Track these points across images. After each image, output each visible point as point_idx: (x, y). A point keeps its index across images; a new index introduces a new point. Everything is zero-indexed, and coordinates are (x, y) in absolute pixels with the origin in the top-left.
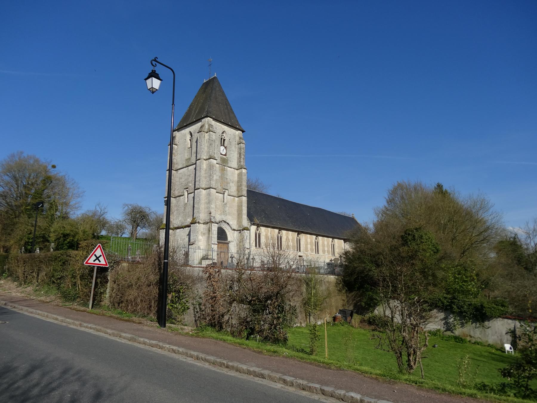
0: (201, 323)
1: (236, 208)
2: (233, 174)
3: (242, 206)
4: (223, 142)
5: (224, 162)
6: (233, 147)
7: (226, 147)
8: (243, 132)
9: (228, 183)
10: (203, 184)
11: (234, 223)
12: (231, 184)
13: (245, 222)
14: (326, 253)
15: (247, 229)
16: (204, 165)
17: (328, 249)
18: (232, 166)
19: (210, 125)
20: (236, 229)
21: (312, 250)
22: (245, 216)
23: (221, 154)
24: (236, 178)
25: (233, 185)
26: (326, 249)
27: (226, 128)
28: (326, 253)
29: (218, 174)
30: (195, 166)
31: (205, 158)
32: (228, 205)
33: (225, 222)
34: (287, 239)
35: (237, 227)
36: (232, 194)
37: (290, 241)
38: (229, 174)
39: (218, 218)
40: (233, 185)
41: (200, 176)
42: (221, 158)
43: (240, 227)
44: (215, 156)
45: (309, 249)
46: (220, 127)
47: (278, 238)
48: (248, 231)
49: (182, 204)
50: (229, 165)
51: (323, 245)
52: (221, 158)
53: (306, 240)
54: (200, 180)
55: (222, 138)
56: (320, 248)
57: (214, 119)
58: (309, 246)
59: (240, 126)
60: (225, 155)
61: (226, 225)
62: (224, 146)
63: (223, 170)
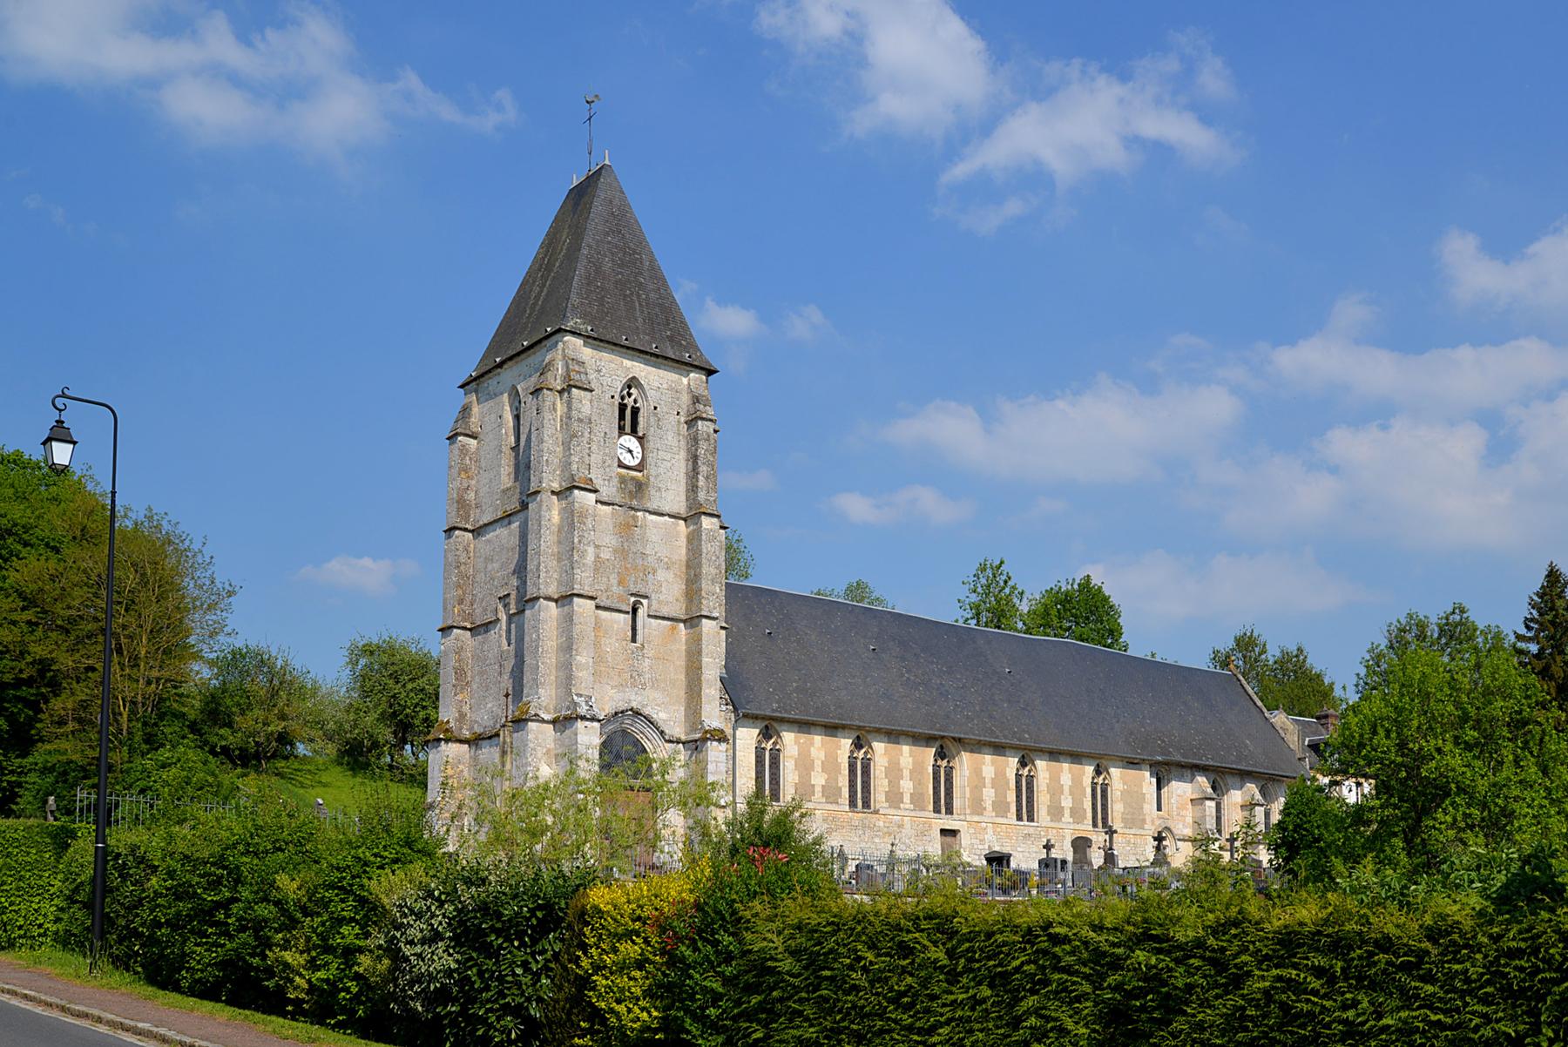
0: (470, 968)
1: (681, 662)
2: (664, 539)
3: (700, 653)
4: (629, 419)
5: (635, 488)
6: (670, 436)
7: (641, 439)
8: (710, 372)
9: (647, 571)
10: (548, 581)
11: (672, 718)
12: (661, 575)
13: (715, 714)
14: (1067, 818)
15: (721, 737)
16: (551, 512)
17: (1077, 802)
18: (666, 509)
19: (572, 361)
20: (683, 738)
21: (917, 800)
22: (712, 692)
23: (621, 465)
24: (684, 551)
25: (670, 576)
26: (1067, 803)
27: (638, 369)
28: (1067, 818)
29: (609, 540)
30: (505, 536)
31: (556, 486)
32: (649, 652)
33: (637, 713)
34: (894, 772)
35: (687, 734)
36: (665, 612)
37: (906, 773)
38: (653, 535)
39: (607, 700)
40: (670, 576)
41: (538, 553)
42: (623, 480)
43: (693, 729)
44: (597, 478)
45: (988, 804)
46: (610, 370)
47: (1018, 783)
48: (724, 746)
49: (492, 655)
50: (652, 506)
51: (1055, 790)
52: (623, 480)
53: (977, 772)
54: (538, 569)
55: (622, 408)
56: (880, 784)
57: (589, 339)
58: (989, 794)
59: (692, 346)
60: (640, 468)
61: (649, 731)
62: (634, 431)
63: (627, 530)
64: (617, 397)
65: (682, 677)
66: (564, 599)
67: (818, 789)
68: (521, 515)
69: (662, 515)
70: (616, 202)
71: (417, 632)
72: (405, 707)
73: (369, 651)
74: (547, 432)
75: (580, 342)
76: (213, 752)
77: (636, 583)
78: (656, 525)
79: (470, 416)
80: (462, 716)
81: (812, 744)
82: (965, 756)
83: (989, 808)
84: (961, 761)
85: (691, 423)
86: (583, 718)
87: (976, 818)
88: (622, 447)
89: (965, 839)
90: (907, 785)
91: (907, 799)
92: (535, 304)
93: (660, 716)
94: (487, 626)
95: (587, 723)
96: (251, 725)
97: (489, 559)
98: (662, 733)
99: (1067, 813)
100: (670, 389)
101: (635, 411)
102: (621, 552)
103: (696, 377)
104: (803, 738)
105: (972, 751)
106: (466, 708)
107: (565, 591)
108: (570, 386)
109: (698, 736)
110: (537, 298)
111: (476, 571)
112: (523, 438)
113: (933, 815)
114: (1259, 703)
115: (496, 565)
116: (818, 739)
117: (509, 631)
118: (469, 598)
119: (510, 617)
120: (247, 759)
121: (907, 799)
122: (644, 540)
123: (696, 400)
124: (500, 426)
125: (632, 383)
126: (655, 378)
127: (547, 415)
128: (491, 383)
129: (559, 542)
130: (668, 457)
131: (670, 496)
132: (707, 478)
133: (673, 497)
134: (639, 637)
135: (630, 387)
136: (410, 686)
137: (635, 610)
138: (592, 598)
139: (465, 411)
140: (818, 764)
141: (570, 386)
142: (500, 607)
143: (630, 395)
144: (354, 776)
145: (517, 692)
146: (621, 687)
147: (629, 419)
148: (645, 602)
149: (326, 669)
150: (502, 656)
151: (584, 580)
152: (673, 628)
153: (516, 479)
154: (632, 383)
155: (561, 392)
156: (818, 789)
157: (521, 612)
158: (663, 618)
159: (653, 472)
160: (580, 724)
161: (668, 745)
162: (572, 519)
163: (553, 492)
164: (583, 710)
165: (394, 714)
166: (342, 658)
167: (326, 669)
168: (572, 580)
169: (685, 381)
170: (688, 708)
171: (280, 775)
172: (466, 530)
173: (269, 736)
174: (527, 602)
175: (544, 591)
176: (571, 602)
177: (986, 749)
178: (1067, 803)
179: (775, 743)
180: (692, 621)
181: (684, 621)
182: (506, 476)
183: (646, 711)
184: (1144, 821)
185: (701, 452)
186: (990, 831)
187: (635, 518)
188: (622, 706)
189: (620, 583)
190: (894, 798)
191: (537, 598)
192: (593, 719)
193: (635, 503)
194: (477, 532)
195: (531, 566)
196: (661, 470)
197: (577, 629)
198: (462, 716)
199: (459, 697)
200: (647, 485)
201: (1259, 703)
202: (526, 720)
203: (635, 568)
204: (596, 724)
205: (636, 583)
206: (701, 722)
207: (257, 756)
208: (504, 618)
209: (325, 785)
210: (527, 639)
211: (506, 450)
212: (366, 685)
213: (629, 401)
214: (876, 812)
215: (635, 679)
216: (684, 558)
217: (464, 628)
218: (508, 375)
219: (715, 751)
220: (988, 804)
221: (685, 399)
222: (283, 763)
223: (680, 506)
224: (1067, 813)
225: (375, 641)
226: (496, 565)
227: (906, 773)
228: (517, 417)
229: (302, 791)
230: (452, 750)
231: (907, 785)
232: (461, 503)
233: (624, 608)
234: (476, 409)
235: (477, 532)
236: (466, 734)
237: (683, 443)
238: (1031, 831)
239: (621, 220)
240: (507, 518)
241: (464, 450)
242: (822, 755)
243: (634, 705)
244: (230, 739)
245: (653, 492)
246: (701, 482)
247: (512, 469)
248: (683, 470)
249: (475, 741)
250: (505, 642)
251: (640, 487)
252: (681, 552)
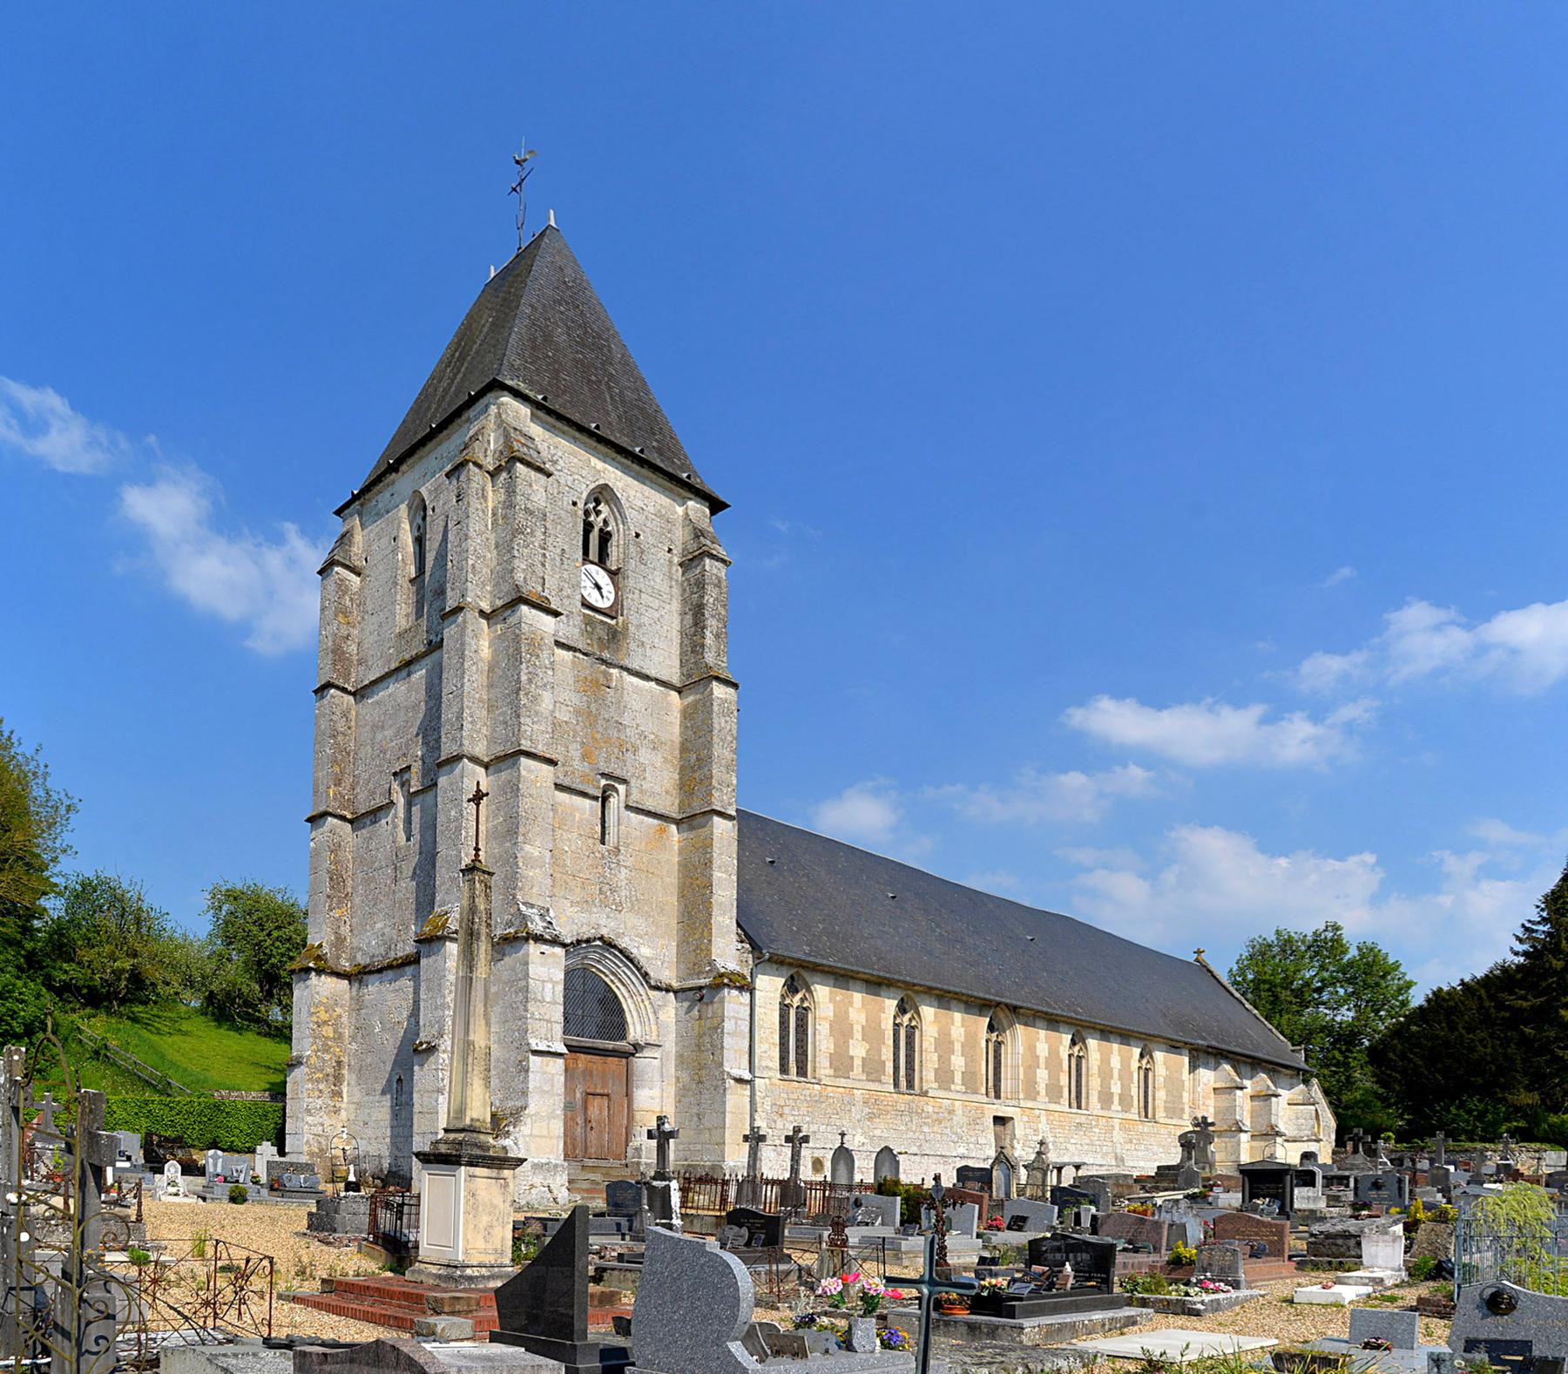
2: (650, 715)
4: (597, 545)
5: (606, 636)
7: (613, 574)
8: (716, 506)
9: (624, 748)
10: (475, 733)
11: (659, 953)
12: (645, 755)
13: (728, 953)
14: (1116, 1106)
16: (481, 642)
17: (1125, 1088)
20: (675, 984)
22: (724, 921)
24: (677, 730)
28: (1116, 1106)
30: (407, 693)
33: (609, 945)
34: (944, 1045)
35: (680, 979)
36: (649, 805)
37: (957, 1046)
42: (588, 622)
45: (1042, 1088)
49: (382, 855)
50: (626, 662)
53: (1031, 1049)
54: (460, 716)
55: (588, 527)
57: (541, 409)
58: (1042, 1075)
61: (625, 971)
62: (602, 561)
63: (596, 688)
64: (581, 505)
65: (674, 900)
66: (506, 759)
67: (858, 1062)
68: (428, 661)
69: (647, 678)
70: (569, 271)
71: (284, 877)
72: (271, 956)
73: (233, 896)
74: (474, 526)
75: (525, 411)
76: (50, 988)
77: (607, 761)
78: (637, 690)
79: (351, 544)
80: (339, 941)
81: (851, 1003)
82: (1020, 1028)
83: (1043, 1092)
84: (1014, 1037)
85: (691, 561)
86: (539, 939)
87: (1030, 1104)
88: (589, 575)
89: (1020, 1128)
90: (958, 1062)
91: (958, 1078)
92: (450, 385)
93: (642, 952)
94: (375, 814)
95: (544, 948)
96: (98, 963)
97: (377, 727)
98: (645, 975)
99: (1116, 1100)
100: (659, 515)
101: (605, 538)
102: (588, 717)
103: (697, 509)
104: (840, 994)
105: (1026, 1024)
106: (345, 930)
107: (499, 750)
108: (514, 459)
109: (703, 982)
110: (446, 391)
111: (359, 745)
112: (430, 558)
113: (985, 1099)
114: (1237, 995)
115: (389, 733)
116: (858, 997)
117: (408, 821)
118: (348, 781)
119: (410, 799)
120: (96, 999)
121: (958, 1078)
122: (622, 708)
123: (698, 533)
124: (394, 551)
125: (602, 494)
126: (639, 498)
127: (475, 504)
128: (382, 498)
129: (491, 686)
130: (656, 604)
131: (657, 656)
132: (717, 636)
133: (660, 651)
134: (611, 838)
135: (598, 502)
136: (275, 934)
137: (605, 800)
138: (551, 762)
139: (345, 539)
140: (857, 1029)
141: (514, 459)
142: (396, 786)
143: (598, 513)
144: (219, 1027)
145: (425, 900)
146: (585, 904)
147: (597, 545)
148: (621, 788)
149: (187, 919)
150: (397, 856)
151: (535, 735)
152: (662, 831)
153: (419, 614)
154: (602, 494)
155: (493, 475)
156: (858, 1062)
157: (431, 786)
158: (649, 813)
159: (633, 619)
160: (533, 949)
161: (652, 993)
162: (514, 650)
163: (482, 612)
164: (537, 926)
165: (260, 963)
166: (204, 900)
167: (187, 919)
168: (517, 733)
169: (680, 510)
170: (683, 942)
171: (135, 1020)
172: (344, 690)
173: (118, 973)
174: (439, 764)
175: (468, 748)
176: (516, 764)
177: (1039, 1023)
178: (1116, 1089)
179: (802, 1000)
180: (693, 819)
181: (678, 822)
182: (403, 612)
183: (623, 943)
184: (1182, 1110)
185: (709, 599)
186: (1043, 1119)
187: (608, 676)
188: (587, 932)
189: (584, 757)
190: (944, 1077)
191: (458, 758)
192: (555, 941)
193: (606, 655)
194: (360, 694)
195: (448, 715)
196: (645, 620)
197: (525, 804)
198: (339, 941)
199: (336, 913)
200: (626, 636)
201: (1237, 995)
202: (443, 939)
203: (608, 741)
204: (559, 951)
205: (607, 761)
206: (711, 963)
207: (109, 997)
208: (400, 800)
209: (185, 1034)
210: (441, 819)
211: (403, 582)
212: (229, 934)
213: (598, 522)
214: (924, 1094)
215: (606, 894)
216: (677, 739)
217: (343, 818)
218: (404, 482)
219: (734, 1003)
220: (1042, 1088)
221: (680, 535)
222: (141, 1008)
223: (674, 675)
224: (1116, 1100)
225: (239, 886)
226: (389, 733)
227: (957, 1046)
228: (420, 541)
229: (155, 1038)
230: (324, 987)
231: (958, 1062)
232: (338, 654)
233: (591, 791)
234: (358, 537)
235: (360, 694)
236: (345, 965)
237: (676, 591)
238: (1083, 1119)
239: (573, 295)
240: (408, 665)
241: (342, 586)
242: (862, 1018)
243: (604, 932)
244: (66, 972)
245: (633, 646)
246: (709, 640)
247: (411, 609)
248: (676, 626)
249: (359, 976)
250: (402, 836)
251: (615, 637)
252: (673, 729)
